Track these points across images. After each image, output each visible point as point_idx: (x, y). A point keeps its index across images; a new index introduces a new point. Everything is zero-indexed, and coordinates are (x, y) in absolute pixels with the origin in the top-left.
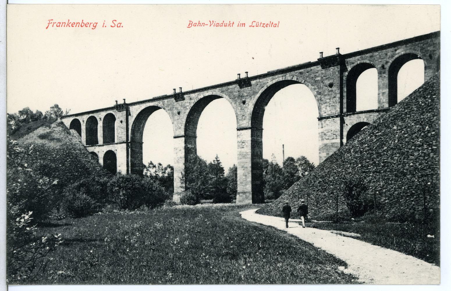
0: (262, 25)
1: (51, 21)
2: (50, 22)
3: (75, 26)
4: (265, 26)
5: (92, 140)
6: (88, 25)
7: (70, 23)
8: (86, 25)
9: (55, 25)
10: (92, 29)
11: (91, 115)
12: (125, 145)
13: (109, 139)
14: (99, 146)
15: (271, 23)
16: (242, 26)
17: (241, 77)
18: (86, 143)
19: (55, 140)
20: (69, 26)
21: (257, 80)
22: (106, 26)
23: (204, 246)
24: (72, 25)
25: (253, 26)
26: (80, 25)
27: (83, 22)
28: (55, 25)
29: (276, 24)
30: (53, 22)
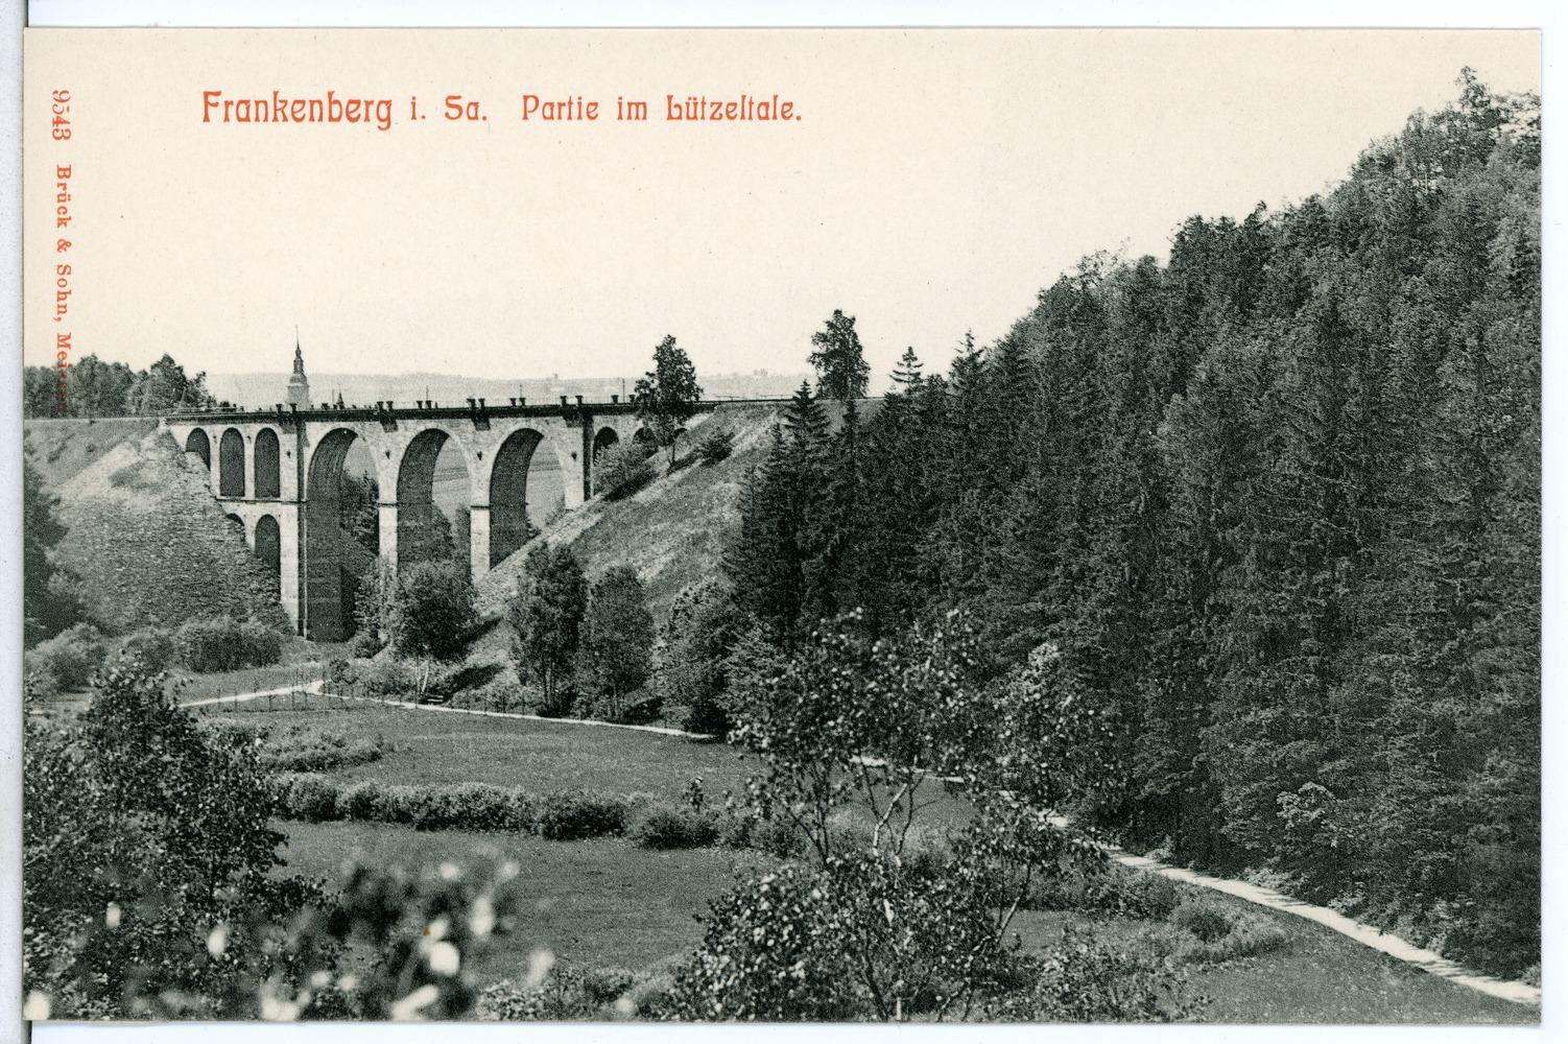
4: (722, 111)
5: (232, 488)
11: (431, 424)
12: (294, 509)
13: (269, 489)
14: (246, 501)
18: (221, 489)
19: (147, 490)
22: (484, 118)
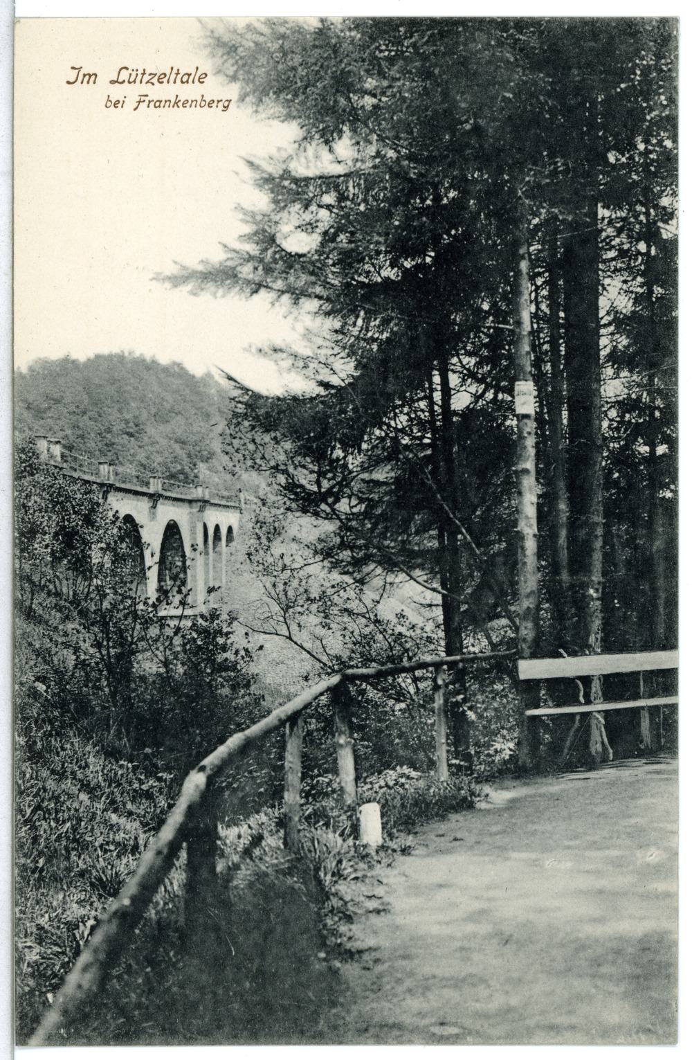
0: (146, 78)
1: (143, 98)
15: (175, 71)
16: (88, 82)
23: (461, 48)
25: (120, 80)
28: (152, 104)
29: (189, 75)
30: (147, 99)
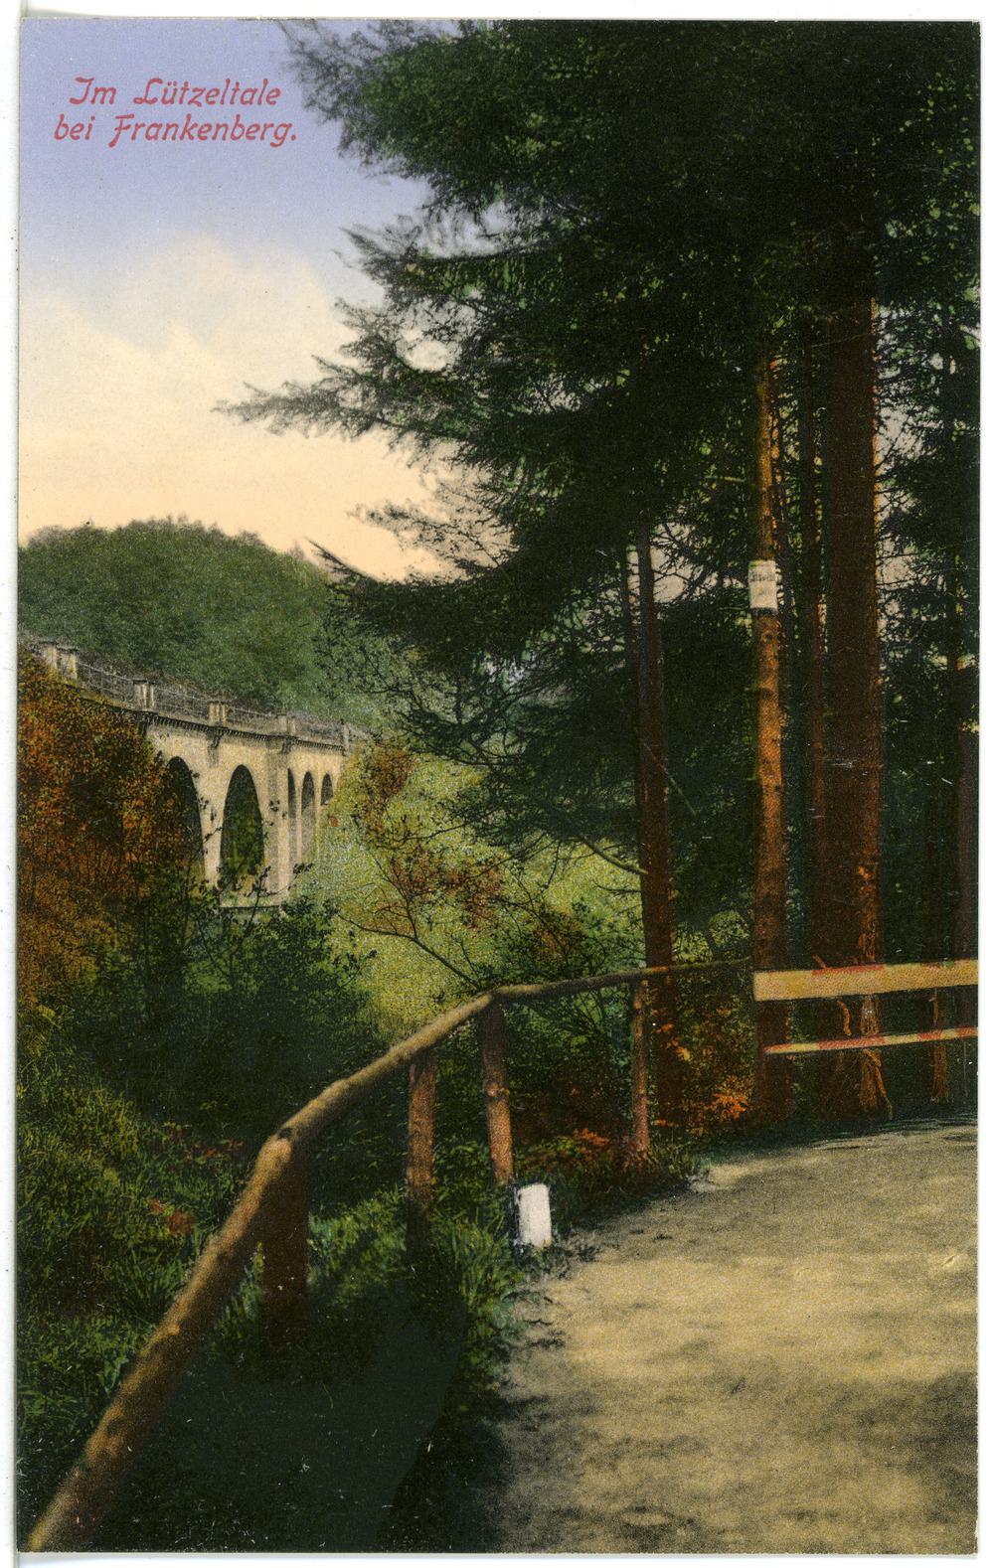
0: (189, 95)
1: (126, 122)
2: (125, 125)
3: (258, 135)
6: (258, 135)
7: (196, 125)
8: (248, 132)
9: (141, 132)
10: (273, 145)
15: (232, 86)
17: (642, 938)
20: (191, 138)
21: (777, 767)
24: (200, 132)
25: (149, 98)
26: (228, 136)
27: (65, 121)
28: (141, 132)
